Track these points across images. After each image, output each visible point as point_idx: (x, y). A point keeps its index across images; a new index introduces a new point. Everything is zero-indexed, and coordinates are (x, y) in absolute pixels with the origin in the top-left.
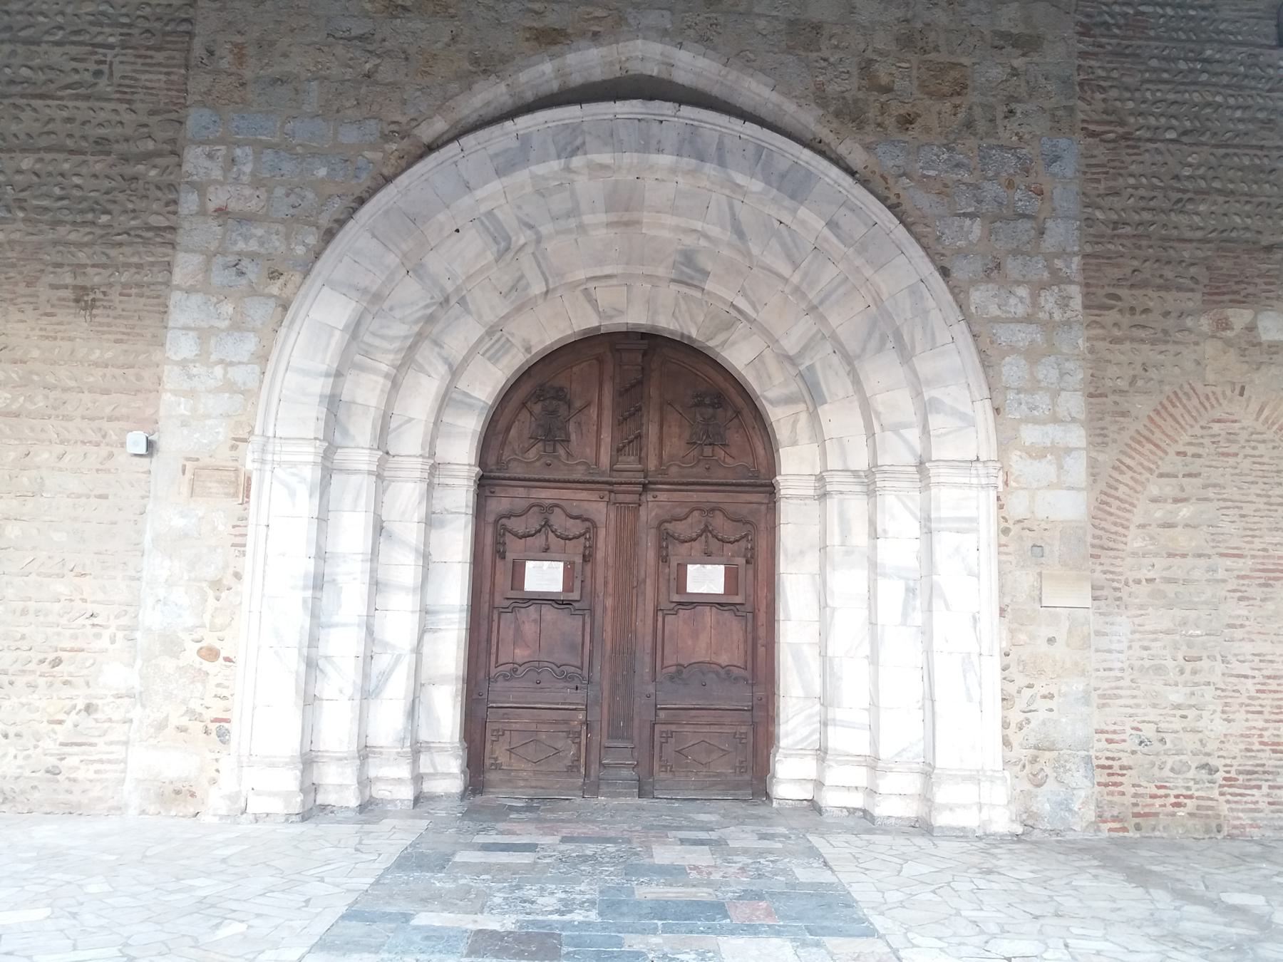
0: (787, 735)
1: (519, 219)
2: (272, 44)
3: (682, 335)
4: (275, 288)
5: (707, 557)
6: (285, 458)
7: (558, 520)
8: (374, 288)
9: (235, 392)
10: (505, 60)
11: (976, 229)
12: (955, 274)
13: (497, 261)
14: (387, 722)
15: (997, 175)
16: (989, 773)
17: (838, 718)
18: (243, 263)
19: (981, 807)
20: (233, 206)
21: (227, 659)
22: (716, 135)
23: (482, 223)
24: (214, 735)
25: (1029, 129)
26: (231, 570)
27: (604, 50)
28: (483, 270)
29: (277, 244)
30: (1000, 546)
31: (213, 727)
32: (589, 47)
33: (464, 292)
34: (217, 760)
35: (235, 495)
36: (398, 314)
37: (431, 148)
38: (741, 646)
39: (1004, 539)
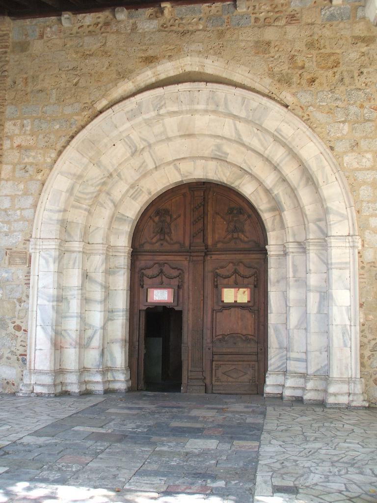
0: (271, 365)
1: (140, 138)
2: (37, 77)
3: (221, 182)
4: (39, 177)
5: (161, 286)
6: (44, 247)
7: (166, 269)
8: (78, 173)
9: (25, 221)
10: (131, 72)
11: (346, 128)
12: (336, 149)
13: (132, 156)
14: (92, 357)
15: (355, 102)
16: (353, 379)
17: (291, 356)
18: (27, 167)
19: (349, 394)
20: (23, 144)
21: (25, 330)
22: (224, 94)
23: (125, 141)
24: (21, 361)
25: (371, 80)
26: (25, 294)
27: (173, 63)
28: (126, 161)
29: (40, 158)
30: (360, 275)
31: (20, 358)
32: (166, 63)
33: (119, 171)
34: (22, 371)
35: (25, 263)
36: (90, 183)
37: (101, 112)
38: (253, 326)
39: (362, 272)
